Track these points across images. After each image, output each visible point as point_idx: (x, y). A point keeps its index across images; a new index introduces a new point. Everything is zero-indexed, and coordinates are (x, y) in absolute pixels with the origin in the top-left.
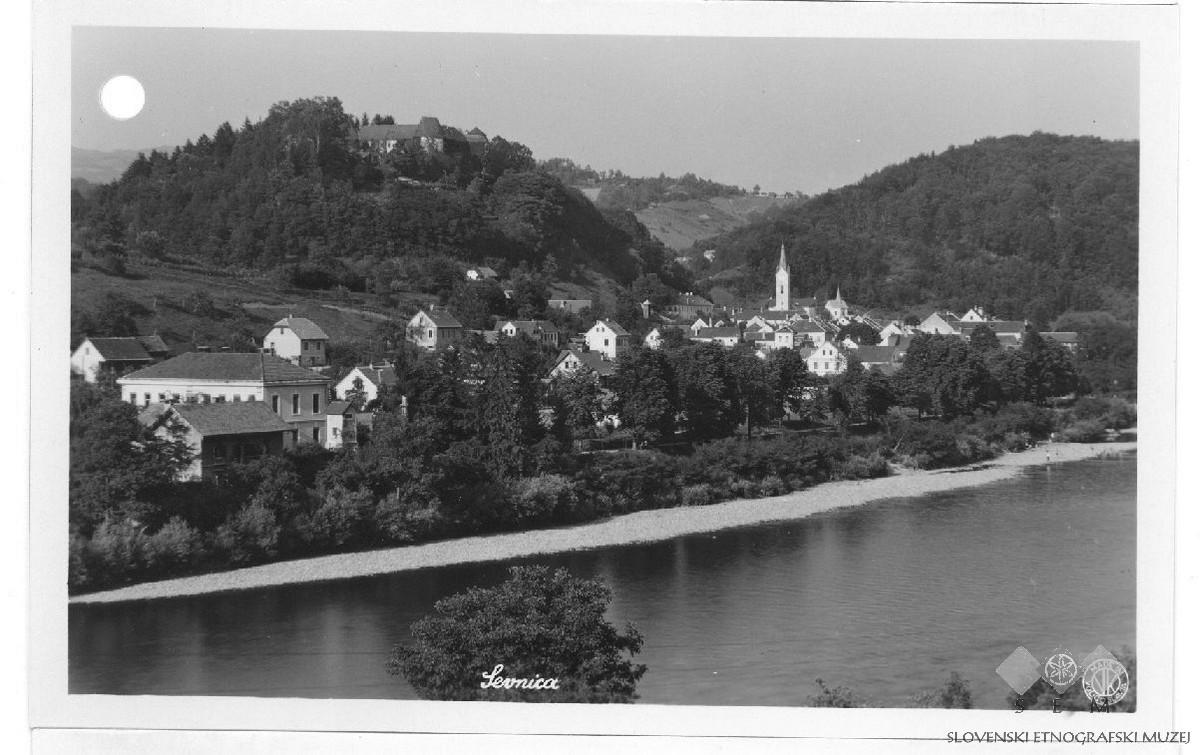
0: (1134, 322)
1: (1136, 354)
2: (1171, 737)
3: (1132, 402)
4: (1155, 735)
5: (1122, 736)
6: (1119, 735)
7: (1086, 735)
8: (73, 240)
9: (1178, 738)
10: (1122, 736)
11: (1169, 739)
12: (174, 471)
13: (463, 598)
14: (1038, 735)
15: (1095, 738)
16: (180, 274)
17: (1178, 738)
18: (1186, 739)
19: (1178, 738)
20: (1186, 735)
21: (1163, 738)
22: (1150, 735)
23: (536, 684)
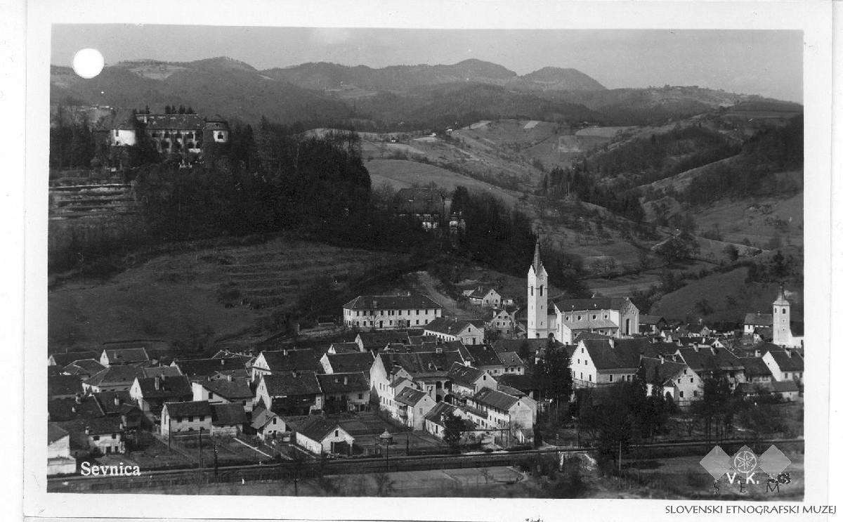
0: (504, 494)
1: (327, 496)
2: (823, 509)
3: (653, 495)
4: (811, 508)
5: (788, 509)
6: (668, 508)
7: (763, 508)
8: (283, 494)
9: (827, 510)
10: (788, 509)
11: (821, 511)
12: (447, 322)
13: (690, 467)
14: (729, 508)
15: (769, 510)
16: (502, 477)
17: (829, 509)
18: (833, 511)
19: (829, 509)
20: (833, 508)
21: (817, 510)
22: (808, 509)
23: (694, 447)
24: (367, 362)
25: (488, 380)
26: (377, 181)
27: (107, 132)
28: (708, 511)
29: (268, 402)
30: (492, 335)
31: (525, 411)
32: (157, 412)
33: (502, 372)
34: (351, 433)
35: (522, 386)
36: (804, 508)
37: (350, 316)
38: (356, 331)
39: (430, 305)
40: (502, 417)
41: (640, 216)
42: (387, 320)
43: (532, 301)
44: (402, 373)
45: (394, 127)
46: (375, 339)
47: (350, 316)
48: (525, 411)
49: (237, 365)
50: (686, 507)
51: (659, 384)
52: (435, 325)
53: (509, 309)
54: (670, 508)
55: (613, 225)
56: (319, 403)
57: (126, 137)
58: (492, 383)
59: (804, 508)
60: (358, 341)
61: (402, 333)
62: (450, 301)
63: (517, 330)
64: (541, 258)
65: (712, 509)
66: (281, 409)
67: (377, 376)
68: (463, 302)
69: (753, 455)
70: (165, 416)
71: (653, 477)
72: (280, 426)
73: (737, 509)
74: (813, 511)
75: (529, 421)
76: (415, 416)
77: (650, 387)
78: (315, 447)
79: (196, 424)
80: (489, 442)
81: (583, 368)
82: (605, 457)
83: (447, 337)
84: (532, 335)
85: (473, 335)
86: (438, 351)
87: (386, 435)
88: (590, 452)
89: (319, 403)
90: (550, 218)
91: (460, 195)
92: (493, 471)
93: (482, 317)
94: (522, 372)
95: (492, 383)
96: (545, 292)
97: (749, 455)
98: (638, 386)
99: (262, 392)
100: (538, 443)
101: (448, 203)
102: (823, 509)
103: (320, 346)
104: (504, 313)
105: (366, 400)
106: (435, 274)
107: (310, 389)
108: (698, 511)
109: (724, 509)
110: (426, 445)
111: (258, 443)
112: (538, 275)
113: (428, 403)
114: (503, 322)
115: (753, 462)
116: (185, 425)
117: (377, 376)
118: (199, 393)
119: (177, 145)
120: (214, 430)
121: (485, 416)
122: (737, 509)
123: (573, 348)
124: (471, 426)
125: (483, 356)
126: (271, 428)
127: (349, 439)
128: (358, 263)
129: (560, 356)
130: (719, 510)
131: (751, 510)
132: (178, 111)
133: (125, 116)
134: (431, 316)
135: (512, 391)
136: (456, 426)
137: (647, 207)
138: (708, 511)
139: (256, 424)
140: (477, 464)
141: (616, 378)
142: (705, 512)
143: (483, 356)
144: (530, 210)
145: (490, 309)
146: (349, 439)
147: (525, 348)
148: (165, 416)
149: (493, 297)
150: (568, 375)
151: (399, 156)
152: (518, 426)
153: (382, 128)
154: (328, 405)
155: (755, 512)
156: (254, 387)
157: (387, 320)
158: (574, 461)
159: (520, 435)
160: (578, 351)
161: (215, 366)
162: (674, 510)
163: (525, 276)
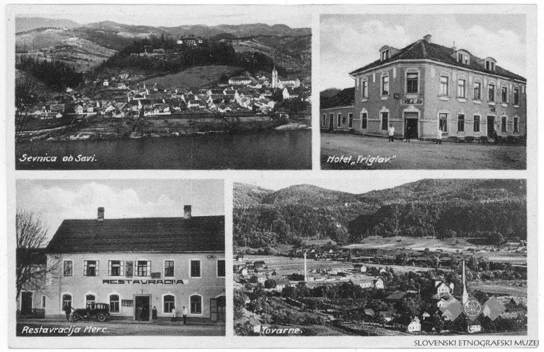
2: (529, 343)
4: (521, 342)
5: (504, 342)
9: (532, 343)
10: (504, 342)
15: (490, 343)
18: (537, 344)
20: (537, 342)
21: (525, 343)
22: (518, 342)
24: (234, 92)
25: (262, 97)
26: (236, 51)
27: (176, 41)
28: (445, 344)
29: (212, 101)
30: (264, 86)
31: (272, 104)
32: (187, 102)
33: (266, 95)
34: (231, 108)
35: (271, 98)
36: (516, 342)
37: (230, 82)
38: (231, 85)
39: (248, 79)
40: (266, 105)
41: (300, 59)
42: (238, 83)
43: (273, 79)
44: (242, 95)
45: (240, 39)
46: (236, 87)
47: (230, 82)
48: (272, 104)
49: (204, 93)
50: (429, 341)
51: (305, 98)
52: (250, 84)
53: (268, 80)
54: (417, 342)
55: (293, 61)
56: (223, 101)
57: (180, 42)
58: (264, 98)
59: (516, 342)
60: (232, 88)
61: (241, 86)
62: (253, 79)
63: (269, 85)
64: (276, 68)
65: (448, 343)
66: (215, 102)
67: (237, 95)
68: (257, 79)
69: (478, 303)
70: (189, 103)
71: (303, 120)
72: (214, 106)
73: (466, 342)
74: (522, 344)
75: (273, 107)
76: (245, 105)
77: (302, 99)
78: (222, 111)
79: (196, 105)
80: (263, 111)
81: (286, 95)
82: (290, 115)
83: (253, 87)
84: (273, 87)
85: (259, 86)
86: (251, 90)
87: (238, 109)
88: (288, 114)
89: (223, 101)
90: (278, 59)
91: (256, 54)
92: (264, 118)
93: (261, 82)
94: (271, 95)
95: (264, 98)
96: (277, 77)
97: (475, 304)
98: (299, 99)
99: (210, 99)
100: (275, 111)
101: (253, 56)
102: (529, 343)
103: (224, 88)
104: (267, 81)
105: (233, 101)
106: (250, 72)
107: (221, 98)
108: (438, 344)
109: (457, 343)
110: (247, 42)
111: (210, 110)
112: (275, 73)
113: (248, 102)
114: (266, 83)
115: (478, 308)
116: (194, 105)
117: (237, 95)
118: (196, 98)
119: (191, 44)
120: (200, 107)
121: (262, 105)
122: (466, 342)
123: (283, 89)
124: (259, 107)
125: (262, 91)
126: (212, 107)
127: (231, 110)
128: (233, 69)
129: (280, 92)
130: (453, 343)
131: (477, 343)
132: (192, 37)
133: (180, 38)
134: (250, 82)
135: (268, 100)
136: (255, 107)
137: (302, 57)
138: (445, 344)
139: (209, 105)
140: (260, 116)
141: (294, 96)
142: (444, 345)
143: (262, 91)
144: (273, 57)
145: (263, 80)
146: (231, 110)
147: (272, 90)
148: (189, 103)
149: (264, 78)
150: (282, 96)
151: (241, 45)
152: (269, 107)
153: (237, 39)
154: (225, 102)
155: (480, 342)
156: (208, 97)
157: (238, 83)
158: (283, 116)
159: (270, 110)
160: (284, 90)
161: (200, 93)
162: (421, 343)
163: (271, 72)
